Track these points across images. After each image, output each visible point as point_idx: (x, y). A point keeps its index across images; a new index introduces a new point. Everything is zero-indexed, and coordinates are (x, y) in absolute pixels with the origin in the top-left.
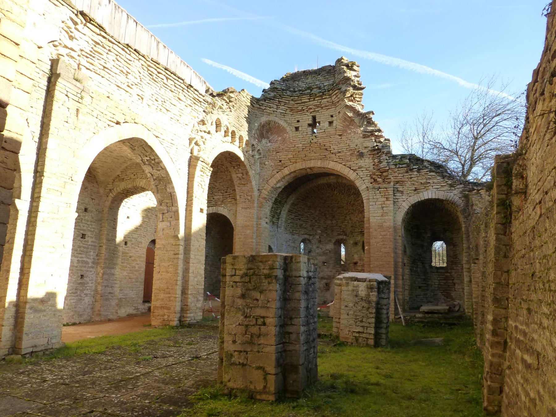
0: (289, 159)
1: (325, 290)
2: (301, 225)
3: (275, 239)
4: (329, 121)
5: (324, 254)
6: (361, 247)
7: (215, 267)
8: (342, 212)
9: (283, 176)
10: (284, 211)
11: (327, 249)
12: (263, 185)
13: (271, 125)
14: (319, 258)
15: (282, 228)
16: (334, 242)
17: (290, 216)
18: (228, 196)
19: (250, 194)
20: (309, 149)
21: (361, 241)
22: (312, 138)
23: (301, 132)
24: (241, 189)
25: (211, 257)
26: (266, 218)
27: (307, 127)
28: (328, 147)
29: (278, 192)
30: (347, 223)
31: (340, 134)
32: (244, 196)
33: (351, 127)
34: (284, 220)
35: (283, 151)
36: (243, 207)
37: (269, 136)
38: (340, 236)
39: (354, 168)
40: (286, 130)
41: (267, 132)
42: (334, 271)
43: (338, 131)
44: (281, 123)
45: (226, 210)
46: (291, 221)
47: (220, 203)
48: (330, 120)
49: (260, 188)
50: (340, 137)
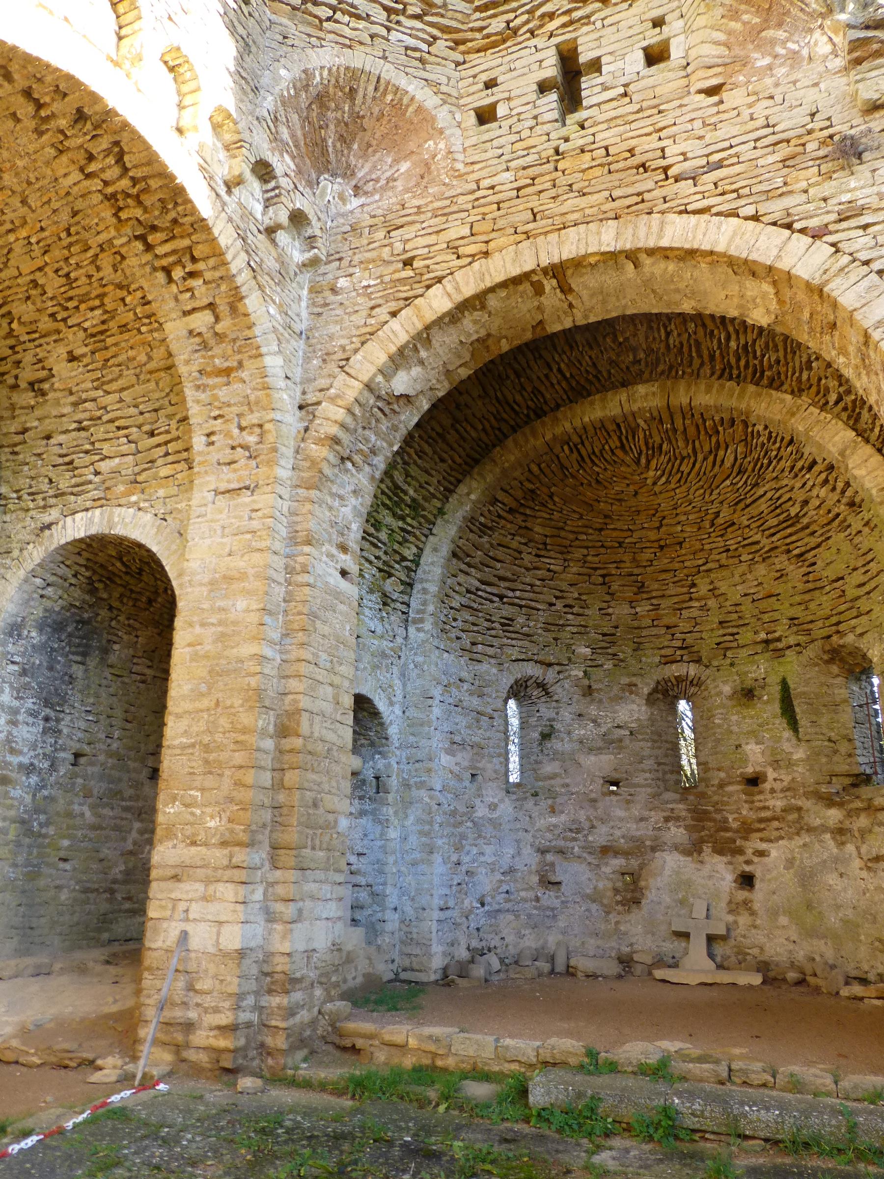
0: (453, 248)
1: (621, 903)
2: (507, 623)
3: (395, 670)
4: (645, 44)
5: (609, 743)
6: (776, 707)
7: (126, 809)
8: (677, 566)
9: (420, 326)
10: (435, 550)
11: (618, 721)
12: (323, 382)
13: (359, 100)
14: (590, 761)
15: (428, 626)
16: (646, 691)
17: (461, 578)
18: (161, 451)
19: (252, 418)
20: (548, 185)
21: (774, 680)
22: (564, 132)
23: (505, 124)
24: (215, 397)
25: (102, 758)
26: (344, 548)
27: (535, 96)
28: (650, 155)
29: (403, 432)
30: (701, 608)
31: (714, 82)
32: (228, 435)
33: (770, 33)
34: (433, 588)
35: (422, 217)
36: (223, 486)
37: (353, 160)
38: (674, 666)
39: (813, 223)
40: (433, 119)
41: (342, 138)
42: (656, 817)
43: (701, 73)
44: (410, 88)
45: (148, 517)
46: (464, 601)
47: (121, 488)
48: (653, 37)
49: (311, 398)
50: (715, 99)
